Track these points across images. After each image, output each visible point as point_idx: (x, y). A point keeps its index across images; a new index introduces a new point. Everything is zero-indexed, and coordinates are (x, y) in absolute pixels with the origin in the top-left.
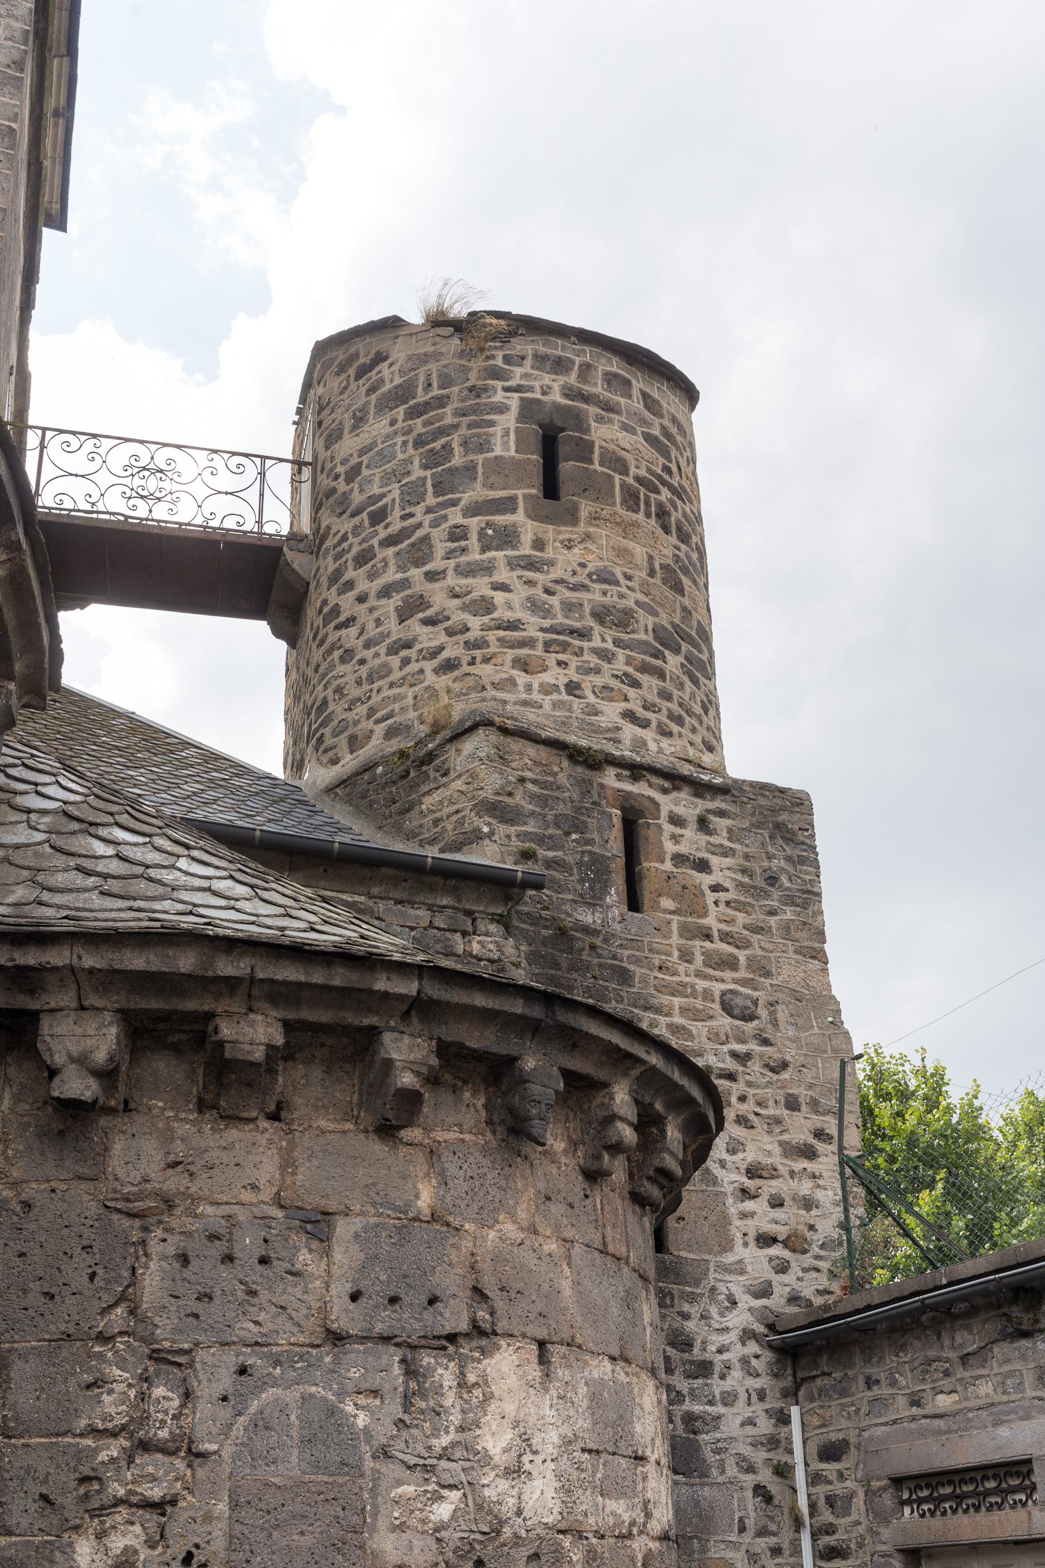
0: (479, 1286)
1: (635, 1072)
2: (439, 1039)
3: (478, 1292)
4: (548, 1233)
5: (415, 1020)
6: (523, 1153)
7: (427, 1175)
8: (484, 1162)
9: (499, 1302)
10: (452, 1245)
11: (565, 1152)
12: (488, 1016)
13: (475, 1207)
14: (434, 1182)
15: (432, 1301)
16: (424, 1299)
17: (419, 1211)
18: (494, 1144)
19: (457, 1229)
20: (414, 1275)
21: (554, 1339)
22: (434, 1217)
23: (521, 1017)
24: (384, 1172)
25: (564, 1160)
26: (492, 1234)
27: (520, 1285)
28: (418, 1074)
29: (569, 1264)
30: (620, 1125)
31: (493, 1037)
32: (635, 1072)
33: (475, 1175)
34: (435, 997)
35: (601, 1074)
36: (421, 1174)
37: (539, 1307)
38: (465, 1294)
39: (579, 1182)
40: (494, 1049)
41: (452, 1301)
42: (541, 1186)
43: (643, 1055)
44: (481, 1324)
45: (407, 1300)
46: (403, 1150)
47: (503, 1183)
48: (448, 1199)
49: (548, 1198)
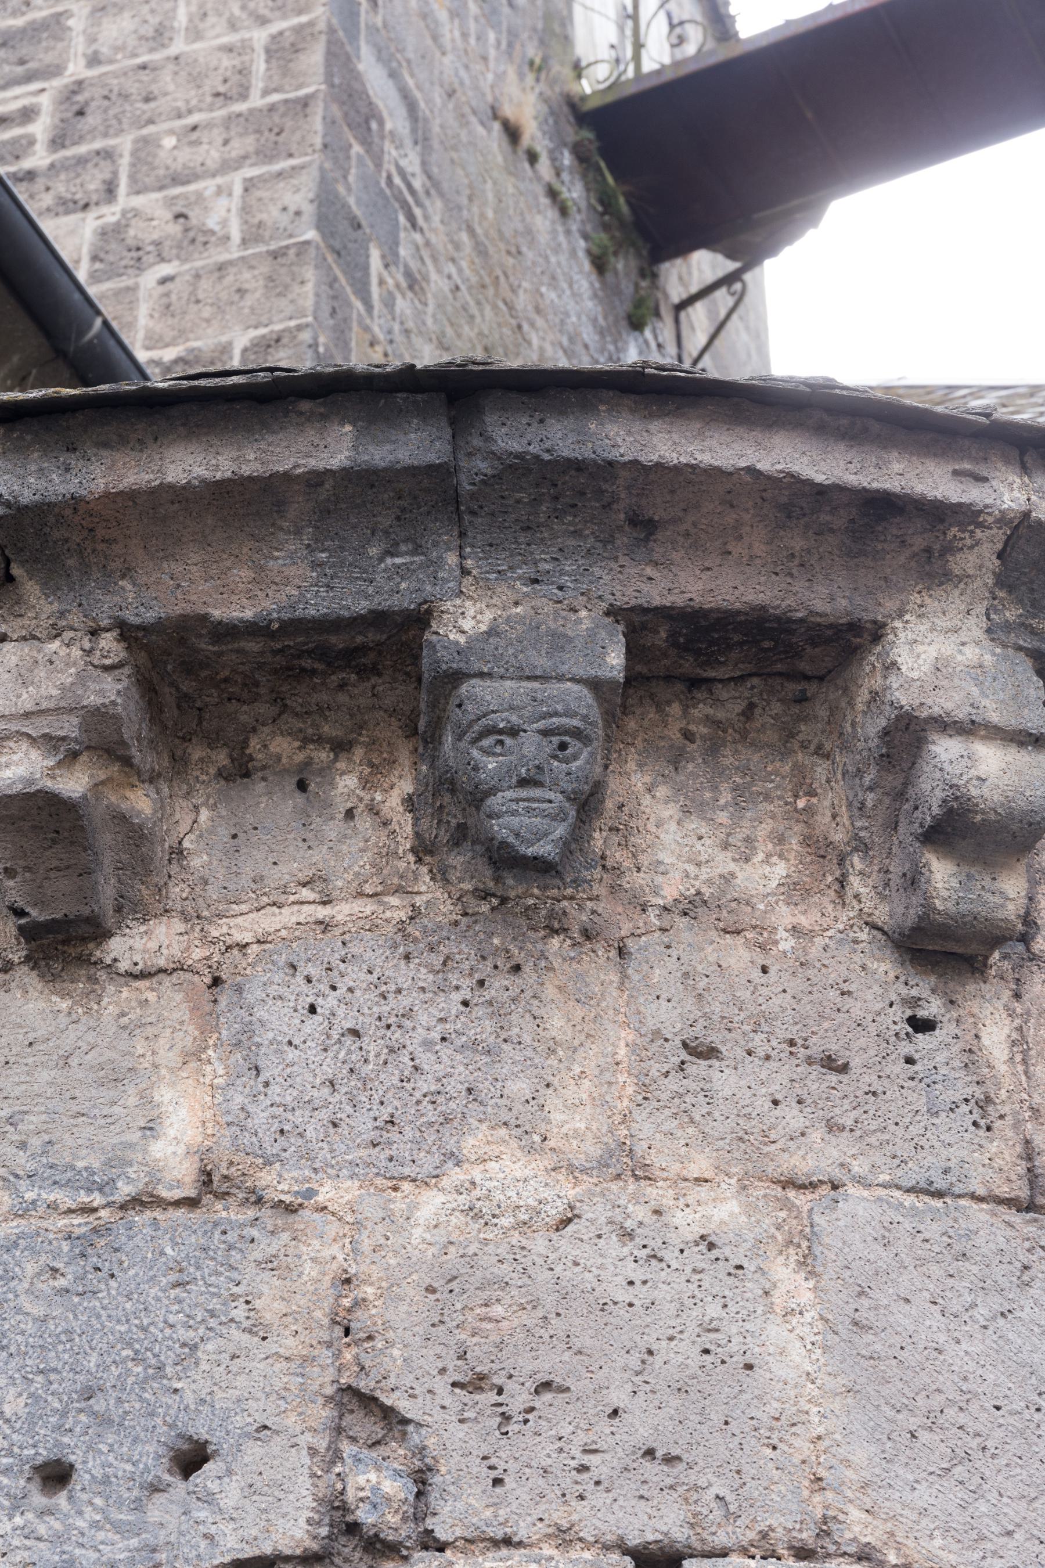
0: (364, 1385)
1: (979, 559)
2: (126, 631)
3: (366, 1409)
4: (700, 1165)
5: (31, 589)
6: (577, 918)
7: (195, 1055)
8: (403, 975)
9: (449, 1431)
10: (269, 1264)
11: (795, 891)
12: (245, 508)
13: (364, 1124)
14: (216, 1070)
15: (191, 1459)
16: (151, 1457)
17: (154, 1176)
18: (446, 909)
19: (290, 1209)
20: (120, 1385)
21: (721, 1539)
22: (210, 1184)
23: (359, 481)
24: (45, 1076)
25: (784, 916)
26: (431, 1204)
27: (550, 1363)
28: (49, 742)
29: (807, 1264)
30: (945, 750)
31: (300, 572)
32: (979, 559)
33: (367, 1023)
34: (27, 497)
35: (821, 596)
36: (168, 1057)
37: (642, 1426)
38: (309, 1420)
39: (880, 984)
40: (317, 605)
41: (253, 1451)
42: (670, 1017)
43: (972, 494)
44: (365, 1516)
45: (88, 1468)
46: (118, 998)
47: (485, 1029)
48: (260, 1117)
49: (703, 1052)
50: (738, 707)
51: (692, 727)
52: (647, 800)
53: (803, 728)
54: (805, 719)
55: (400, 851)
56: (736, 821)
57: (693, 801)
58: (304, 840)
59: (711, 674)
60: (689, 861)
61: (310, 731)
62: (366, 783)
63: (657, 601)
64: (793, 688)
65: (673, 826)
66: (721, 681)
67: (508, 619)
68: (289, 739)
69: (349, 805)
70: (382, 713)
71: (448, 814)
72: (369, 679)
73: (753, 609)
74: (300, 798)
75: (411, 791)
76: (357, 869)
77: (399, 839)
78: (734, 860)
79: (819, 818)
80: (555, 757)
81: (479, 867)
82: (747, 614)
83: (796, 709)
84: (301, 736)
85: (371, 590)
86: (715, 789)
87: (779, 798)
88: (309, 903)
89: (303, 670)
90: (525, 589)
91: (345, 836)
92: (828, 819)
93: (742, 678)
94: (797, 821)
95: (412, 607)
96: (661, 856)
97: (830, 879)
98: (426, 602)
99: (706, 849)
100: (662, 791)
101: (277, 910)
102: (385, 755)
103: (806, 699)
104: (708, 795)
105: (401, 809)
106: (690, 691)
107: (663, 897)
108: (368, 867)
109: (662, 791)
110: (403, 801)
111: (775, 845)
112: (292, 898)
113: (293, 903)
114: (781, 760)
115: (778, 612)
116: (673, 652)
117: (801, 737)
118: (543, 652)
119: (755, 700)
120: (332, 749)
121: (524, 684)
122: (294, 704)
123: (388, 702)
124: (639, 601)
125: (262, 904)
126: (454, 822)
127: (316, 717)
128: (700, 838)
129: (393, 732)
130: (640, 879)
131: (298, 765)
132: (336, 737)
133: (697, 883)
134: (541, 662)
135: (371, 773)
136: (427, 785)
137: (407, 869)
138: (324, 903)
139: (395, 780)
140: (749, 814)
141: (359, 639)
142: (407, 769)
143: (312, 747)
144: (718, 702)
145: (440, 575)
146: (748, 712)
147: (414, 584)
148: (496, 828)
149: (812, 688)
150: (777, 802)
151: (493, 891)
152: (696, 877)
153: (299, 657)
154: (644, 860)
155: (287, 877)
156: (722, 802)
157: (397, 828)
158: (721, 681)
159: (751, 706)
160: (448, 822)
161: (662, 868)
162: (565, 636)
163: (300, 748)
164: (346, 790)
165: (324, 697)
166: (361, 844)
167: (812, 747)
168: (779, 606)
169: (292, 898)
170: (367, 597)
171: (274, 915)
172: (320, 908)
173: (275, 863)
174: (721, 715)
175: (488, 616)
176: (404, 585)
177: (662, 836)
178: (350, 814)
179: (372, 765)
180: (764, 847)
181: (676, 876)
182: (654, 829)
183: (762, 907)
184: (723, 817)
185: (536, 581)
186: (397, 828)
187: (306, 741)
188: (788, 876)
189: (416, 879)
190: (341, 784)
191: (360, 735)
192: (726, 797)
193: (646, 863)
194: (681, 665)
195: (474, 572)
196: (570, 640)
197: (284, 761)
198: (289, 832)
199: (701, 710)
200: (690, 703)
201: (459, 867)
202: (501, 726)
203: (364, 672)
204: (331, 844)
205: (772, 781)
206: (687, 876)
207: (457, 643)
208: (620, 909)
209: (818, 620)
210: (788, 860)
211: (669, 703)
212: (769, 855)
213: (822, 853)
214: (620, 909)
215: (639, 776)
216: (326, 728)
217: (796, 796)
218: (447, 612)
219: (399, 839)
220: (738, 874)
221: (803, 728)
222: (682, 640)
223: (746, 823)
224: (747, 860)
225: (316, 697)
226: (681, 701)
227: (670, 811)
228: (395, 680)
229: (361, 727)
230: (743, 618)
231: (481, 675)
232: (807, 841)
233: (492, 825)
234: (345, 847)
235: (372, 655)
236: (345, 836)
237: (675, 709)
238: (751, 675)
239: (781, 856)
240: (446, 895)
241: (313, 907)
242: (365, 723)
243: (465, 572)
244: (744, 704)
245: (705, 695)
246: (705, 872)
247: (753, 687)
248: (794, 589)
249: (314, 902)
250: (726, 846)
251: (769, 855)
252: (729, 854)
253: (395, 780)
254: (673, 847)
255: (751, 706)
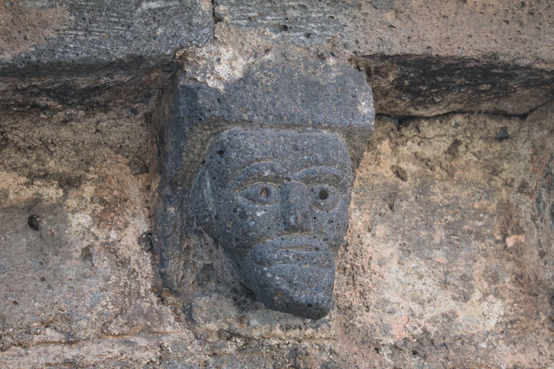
50: (445, 145)
51: (403, 165)
52: (367, 239)
53: (506, 166)
54: (507, 157)
55: (142, 291)
56: (452, 258)
57: (410, 240)
58: (43, 279)
59: (422, 112)
60: (413, 299)
61: (35, 166)
62: (99, 220)
63: (397, 50)
64: (494, 125)
65: (394, 266)
66: (427, 118)
67: (262, 67)
68: (14, 174)
69: (85, 244)
70: (108, 149)
71: (194, 256)
72: (94, 114)
73: (484, 57)
74: (32, 235)
75: (146, 230)
76: (100, 309)
77: (139, 279)
78: (454, 298)
79: (527, 256)
80: (317, 205)
81: (225, 308)
82: (478, 61)
83: (498, 147)
84: (27, 171)
85: (129, 36)
86: (429, 226)
87: (491, 236)
88: (55, 343)
89: (35, 106)
90: (274, 36)
91: (84, 276)
92: (536, 257)
93: (447, 116)
94: (508, 259)
95: (169, 52)
96: (386, 295)
97: (543, 318)
98: (182, 47)
99: (428, 287)
100: (381, 230)
101: (23, 351)
102: (116, 193)
103: (507, 137)
104: (423, 233)
105: (138, 248)
106: (399, 129)
107: (392, 336)
108: (110, 307)
109: (381, 230)
110: (140, 240)
111: (490, 284)
112: (36, 338)
113: (38, 343)
114: (487, 198)
115: (507, 59)
116: (393, 93)
117: (504, 175)
118: (298, 101)
119: (459, 137)
120: (60, 186)
121: (283, 131)
122: (16, 139)
123: (114, 138)
124: (381, 49)
125: (7, 344)
126: (200, 263)
127: (41, 152)
128: (421, 277)
129: (121, 169)
130: (369, 318)
131: (26, 201)
132: (64, 173)
133: (422, 322)
134: (295, 108)
135: (104, 211)
136: (175, 226)
137: (151, 309)
138: (70, 343)
139: (129, 219)
140: (463, 253)
141: (104, 80)
142: (139, 207)
143: (39, 183)
144: (424, 140)
145: (195, 20)
146: (453, 150)
147: (170, 30)
148: (269, 275)
149: (512, 126)
150: (488, 241)
151: (238, 331)
152: (421, 316)
153: (38, 95)
154: (372, 298)
155: (29, 316)
156: (437, 240)
157: (136, 267)
158: (427, 118)
159: (456, 143)
160: (194, 263)
161: (388, 308)
162: (317, 83)
163: (27, 184)
164: (80, 228)
165: (47, 131)
166: (102, 284)
167: (516, 185)
168: (508, 54)
169: (36, 338)
170: (126, 42)
171: (20, 355)
172: (66, 348)
173: (15, 303)
174: (428, 152)
175: (240, 64)
176: (160, 31)
177: (385, 275)
178: (87, 254)
179: (103, 202)
180: (481, 285)
181: (403, 314)
182: (377, 269)
183: (484, 345)
184: (440, 256)
185: (285, 28)
186: (136, 267)
187: (32, 177)
188: (505, 315)
189: (161, 319)
190: (74, 222)
191: (87, 171)
192: (440, 235)
193: (374, 302)
194: (396, 105)
195: (226, 18)
196: (322, 88)
197: (11, 197)
198: (26, 271)
199: (409, 148)
200: (399, 140)
201: (205, 308)
202: (266, 174)
203: (91, 108)
204: (71, 284)
205: (481, 220)
206: (413, 315)
207: (216, 90)
208: (355, 349)
209: (543, 66)
210: (503, 299)
211: (380, 140)
212: (485, 295)
213: (534, 291)
214: (355, 349)
215: (358, 213)
216: (52, 164)
217: (505, 236)
218: (203, 57)
219: (139, 279)
220: (459, 313)
221: (506, 166)
222: (406, 83)
223: (461, 262)
224: (466, 299)
225: (37, 132)
226: (390, 138)
227: (390, 250)
228: (120, 116)
229: (88, 163)
230: (472, 65)
231: (243, 122)
232: (519, 279)
233: (264, 273)
234: (85, 287)
235: (107, 94)
236: (84, 276)
237: (385, 146)
238: (454, 113)
239: (496, 295)
240: (192, 336)
241: (59, 347)
242: (93, 159)
243: (218, 19)
244: (450, 141)
245: (413, 132)
246: (430, 312)
247: (457, 125)
248: (523, 37)
249: (60, 342)
250: (445, 284)
251: (485, 295)
252: (449, 293)
253: (129, 219)
254: (397, 285)
255: (456, 143)
